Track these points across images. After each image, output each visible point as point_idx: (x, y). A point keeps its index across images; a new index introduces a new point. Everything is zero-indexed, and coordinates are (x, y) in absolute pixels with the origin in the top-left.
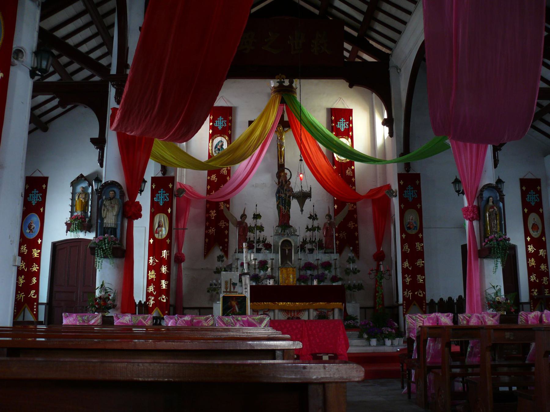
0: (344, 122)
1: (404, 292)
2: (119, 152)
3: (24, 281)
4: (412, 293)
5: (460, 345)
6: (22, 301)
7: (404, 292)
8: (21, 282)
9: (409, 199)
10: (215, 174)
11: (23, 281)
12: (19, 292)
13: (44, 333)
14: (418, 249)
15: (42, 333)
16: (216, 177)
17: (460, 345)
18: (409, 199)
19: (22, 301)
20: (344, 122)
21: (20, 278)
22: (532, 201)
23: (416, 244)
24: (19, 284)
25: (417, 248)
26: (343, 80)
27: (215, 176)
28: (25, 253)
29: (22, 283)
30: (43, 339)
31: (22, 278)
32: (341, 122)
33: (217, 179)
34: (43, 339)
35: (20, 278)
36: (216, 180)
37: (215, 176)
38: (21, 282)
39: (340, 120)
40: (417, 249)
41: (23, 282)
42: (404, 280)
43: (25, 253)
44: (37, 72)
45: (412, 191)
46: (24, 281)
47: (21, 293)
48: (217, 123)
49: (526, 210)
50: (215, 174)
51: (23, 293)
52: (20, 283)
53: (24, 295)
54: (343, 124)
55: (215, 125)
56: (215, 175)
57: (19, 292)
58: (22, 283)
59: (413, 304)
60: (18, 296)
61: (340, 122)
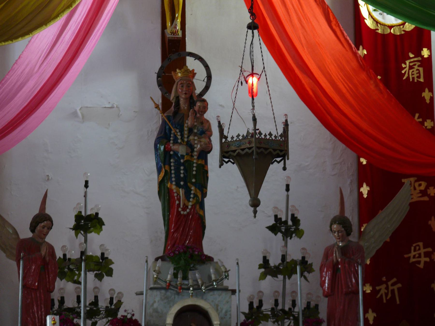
6: (398, 302)
19: (398, 302)
51: (395, 280)
53: (399, 285)
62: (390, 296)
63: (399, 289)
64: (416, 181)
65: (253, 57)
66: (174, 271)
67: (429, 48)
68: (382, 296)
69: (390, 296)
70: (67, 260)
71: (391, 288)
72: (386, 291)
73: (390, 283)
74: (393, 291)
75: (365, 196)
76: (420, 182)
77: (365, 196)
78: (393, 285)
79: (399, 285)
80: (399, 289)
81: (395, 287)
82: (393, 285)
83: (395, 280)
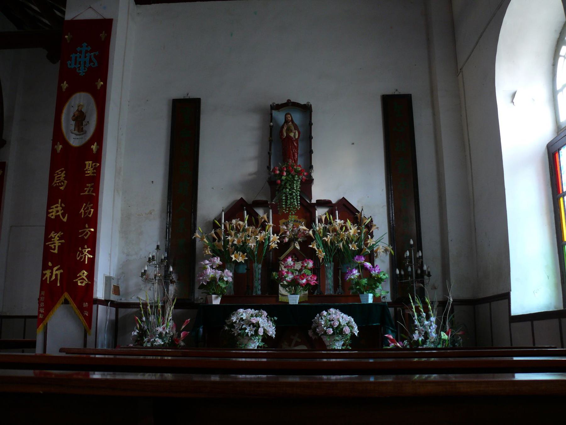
1: (44, 272)
2: (564, 15)
3: (63, 241)
4: (62, 271)
7: (44, 272)
9: (79, 70)
12: (50, 264)
13: (231, 352)
14: (89, 174)
15: (170, 350)
18: (79, 70)
22: (79, 68)
23: (85, 165)
25: (86, 170)
28: (61, 188)
30: (265, 360)
34: (265, 360)
39: (79, 49)
40: (86, 172)
41: (60, 244)
42: (47, 244)
43: (61, 188)
45: (87, 55)
46: (63, 241)
47: (54, 266)
48: (73, 59)
49: (65, 85)
52: (55, 246)
53: (62, 271)
55: (70, 65)
57: (50, 264)
59: (62, 300)
60: (48, 272)
64: (92, 163)
69: (54, 277)
71: (54, 273)
80: (61, 273)
82: (56, 270)
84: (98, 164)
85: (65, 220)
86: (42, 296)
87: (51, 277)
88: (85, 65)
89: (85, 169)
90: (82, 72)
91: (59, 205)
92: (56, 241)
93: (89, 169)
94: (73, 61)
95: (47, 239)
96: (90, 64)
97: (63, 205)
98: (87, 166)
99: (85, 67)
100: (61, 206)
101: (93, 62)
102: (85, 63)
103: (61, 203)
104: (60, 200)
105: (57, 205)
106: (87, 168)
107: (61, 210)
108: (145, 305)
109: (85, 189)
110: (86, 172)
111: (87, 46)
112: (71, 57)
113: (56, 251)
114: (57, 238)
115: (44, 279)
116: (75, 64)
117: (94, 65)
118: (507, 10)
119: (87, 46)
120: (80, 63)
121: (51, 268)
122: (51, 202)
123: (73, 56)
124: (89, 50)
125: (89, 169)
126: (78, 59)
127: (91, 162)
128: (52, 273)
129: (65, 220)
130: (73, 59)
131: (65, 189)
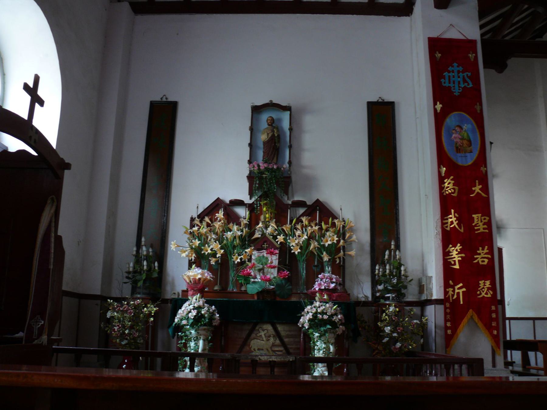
0: (459, 72)
5: (25, 332)
6: (462, 303)
8: (457, 259)
10: (452, 177)
11: (460, 255)
12: (451, 282)
14: (479, 229)
16: (454, 185)
17: (25, 332)
19: (462, 303)
20: (459, 72)
21: (451, 249)
22: (454, 87)
24: (453, 263)
26: (393, 16)
27: (453, 182)
29: (459, 260)
31: (457, 250)
32: (453, 72)
33: (456, 188)
35: (451, 249)
36: (457, 191)
37: (453, 182)
38: (457, 259)
39: (450, 69)
40: (476, 228)
41: (460, 259)
44: (106, 330)
46: (463, 255)
48: (447, 78)
49: (439, 106)
50: (452, 177)
51: (461, 285)
52: (455, 261)
53: (464, 289)
54: (459, 77)
55: (445, 83)
56: (451, 180)
57: (451, 282)
58: (459, 260)
61: (449, 72)
62: (455, 297)
63: (463, 292)
64: (482, 216)
65: (291, 168)
66: (486, 171)
67: (435, 110)
68: (449, 296)
69: (455, 297)
70: (210, 279)
71: (457, 291)
72: (453, 293)
73: (456, 287)
74: (458, 293)
75: (331, 327)
76: (486, 217)
77: (331, 327)
78: (459, 289)
79: (464, 289)
80: (463, 292)
81: (461, 291)
82: (459, 289)
83: (461, 285)
84: (487, 218)
85: (462, 230)
86: (448, 321)
87: (453, 296)
88: (460, 85)
89: (474, 224)
90: (457, 91)
91: (453, 217)
92: (455, 254)
93: (478, 224)
94: (447, 81)
95: (446, 254)
96: (464, 84)
97: (456, 215)
98: (476, 220)
99: (459, 87)
100: (455, 217)
101: (467, 82)
102: (459, 83)
103: (455, 213)
104: (453, 211)
105: (451, 216)
106: (475, 223)
107: (456, 221)
108: (481, 27)
109: (476, 257)
110: (476, 228)
111: (458, 67)
112: (445, 76)
113: (457, 267)
114: (455, 253)
115: (447, 297)
116: (450, 83)
117: (468, 85)
118: (373, 16)
119: (458, 67)
120: (454, 82)
121: (453, 287)
122: (444, 213)
123: (446, 74)
124: (461, 71)
125: (478, 224)
126: (452, 79)
127: (480, 215)
128: (454, 291)
129: (462, 230)
130: (447, 78)
131: (449, 246)
